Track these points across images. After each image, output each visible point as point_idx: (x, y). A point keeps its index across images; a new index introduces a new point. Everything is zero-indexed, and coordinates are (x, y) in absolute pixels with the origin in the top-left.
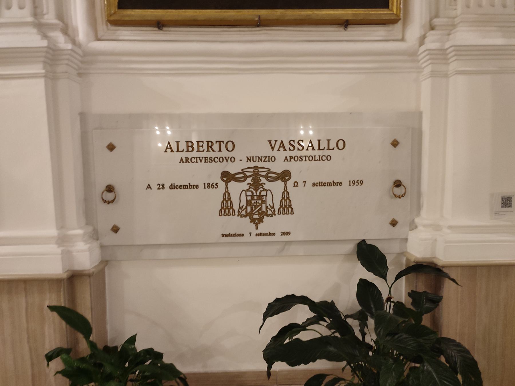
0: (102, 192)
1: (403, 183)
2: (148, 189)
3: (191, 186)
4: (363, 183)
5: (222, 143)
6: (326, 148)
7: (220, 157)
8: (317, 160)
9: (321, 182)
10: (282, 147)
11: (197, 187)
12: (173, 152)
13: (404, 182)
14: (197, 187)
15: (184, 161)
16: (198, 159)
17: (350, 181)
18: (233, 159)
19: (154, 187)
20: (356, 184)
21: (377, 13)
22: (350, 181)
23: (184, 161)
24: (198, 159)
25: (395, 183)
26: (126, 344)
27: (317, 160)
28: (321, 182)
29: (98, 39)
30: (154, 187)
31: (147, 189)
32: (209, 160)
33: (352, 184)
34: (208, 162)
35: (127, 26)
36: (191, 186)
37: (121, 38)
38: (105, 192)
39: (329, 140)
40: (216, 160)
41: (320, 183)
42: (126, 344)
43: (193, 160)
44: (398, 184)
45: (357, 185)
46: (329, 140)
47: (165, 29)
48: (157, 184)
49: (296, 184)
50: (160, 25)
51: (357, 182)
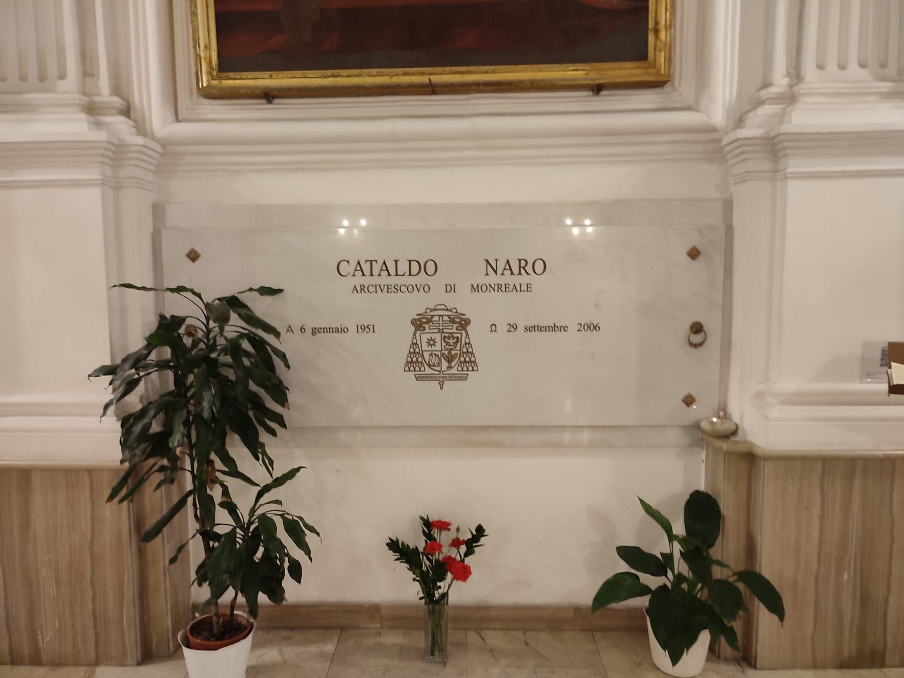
0: (707, 336)
1: (705, 329)
2: (288, 332)
3: (554, 328)
4: (300, 328)
5: (374, 263)
6: (408, 273)
7: (425, 284)
8: (524, 291)
9: (536, 325)
10: (384, 270)
11: (565, 328)
12: (365, 275)
13: (707, 327)
14: (565, 328)
15: (359, 290)
16: (378, 287)
17: (357, 326)
18: (426, 288)
19: (502, 328)
20: (367, 330)
21: (739, 59)
22: (357, 326)
23: (359, 290)
24: (378, 287)
25: (692, 328)
26: (198, 575)
27: (524, 291)
28: (536, 325)
29: (178, 120)
30: (296, 329)
31: (287, 332)
32: (393, 288)
33: (371, 328)
34: (509, 291)
35: (557, 91)
36: (554, 328)
37: (204, 117)
38: (692, 335)
39: (396, 261)
40: (403, 289)
41: (535, 326)
42: (198, 575)
43: (371, 289)
44: (697, 328)
45: (367, 332)
46: (396, 261)
47: (276, 101)
48: (578, 323)
49: (493, 327)
50: (269, 96)
51: (367, 327)
